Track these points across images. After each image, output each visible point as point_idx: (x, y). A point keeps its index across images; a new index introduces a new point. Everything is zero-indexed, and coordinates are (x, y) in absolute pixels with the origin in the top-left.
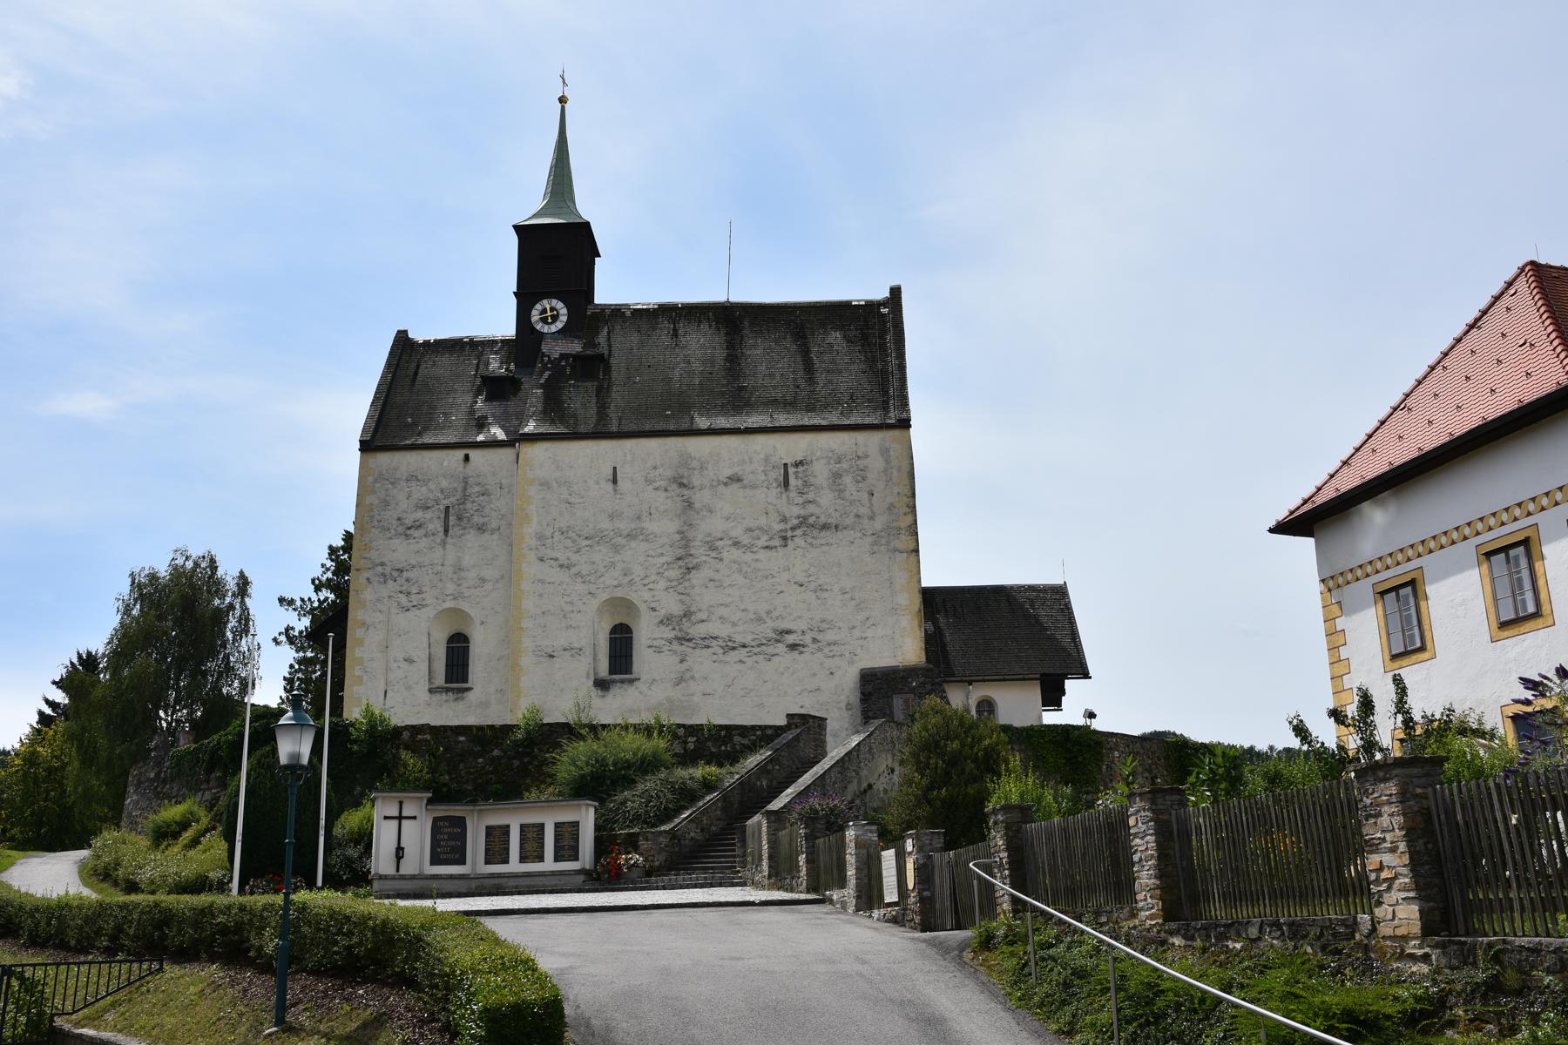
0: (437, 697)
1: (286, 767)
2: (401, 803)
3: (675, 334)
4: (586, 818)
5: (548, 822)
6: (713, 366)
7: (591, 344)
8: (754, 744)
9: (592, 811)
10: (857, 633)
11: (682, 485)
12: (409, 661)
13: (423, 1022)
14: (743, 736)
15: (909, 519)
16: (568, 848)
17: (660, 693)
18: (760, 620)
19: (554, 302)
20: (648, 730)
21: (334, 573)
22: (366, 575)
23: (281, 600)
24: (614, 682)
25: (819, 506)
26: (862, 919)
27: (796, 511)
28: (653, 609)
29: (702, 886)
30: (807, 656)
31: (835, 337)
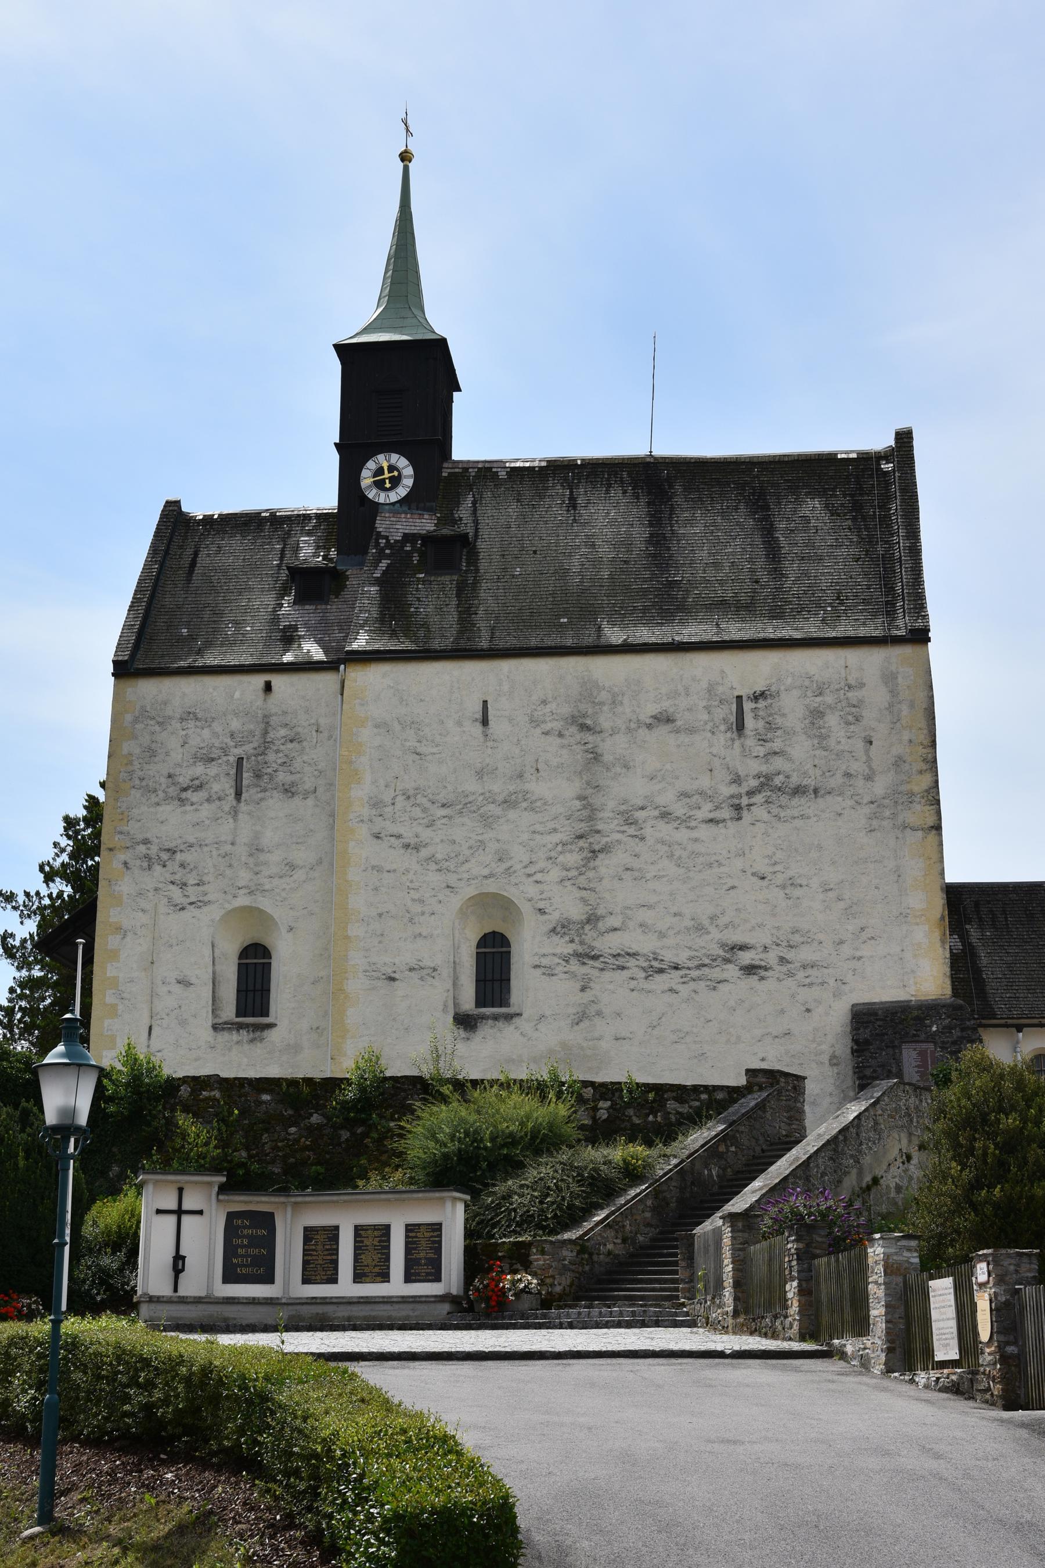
0: (225, 1037)
1: (55, 1129)
2: (181, 1190)
3: (573, 504)
4: (452, 1217)
5: (397, 1221)
6: (629, 551)
7: (448, 519)
8: (698, 1112)
9: (460, 1208)
10: (846, 950)
11: (584, 728)
12: (184, 982)
13: (274, 1529)
14: (680, 1100)
15: (926, 780)
16: (424, 1262)
17: (537, 1042)
18: (700, 929)
19: (394, 458)
20: (539, 1089)
21: (71, 856)
22: (122, 857)
23: (485, 702)
24: (484, 1017)
25: (790, 760)
26: (897, 1382)
27: (755, 767)
28: (542, 912)
29: (629, 1325)
30: (770, 984)
31: (813, 507)
